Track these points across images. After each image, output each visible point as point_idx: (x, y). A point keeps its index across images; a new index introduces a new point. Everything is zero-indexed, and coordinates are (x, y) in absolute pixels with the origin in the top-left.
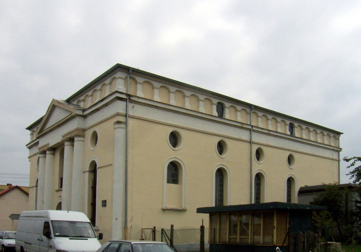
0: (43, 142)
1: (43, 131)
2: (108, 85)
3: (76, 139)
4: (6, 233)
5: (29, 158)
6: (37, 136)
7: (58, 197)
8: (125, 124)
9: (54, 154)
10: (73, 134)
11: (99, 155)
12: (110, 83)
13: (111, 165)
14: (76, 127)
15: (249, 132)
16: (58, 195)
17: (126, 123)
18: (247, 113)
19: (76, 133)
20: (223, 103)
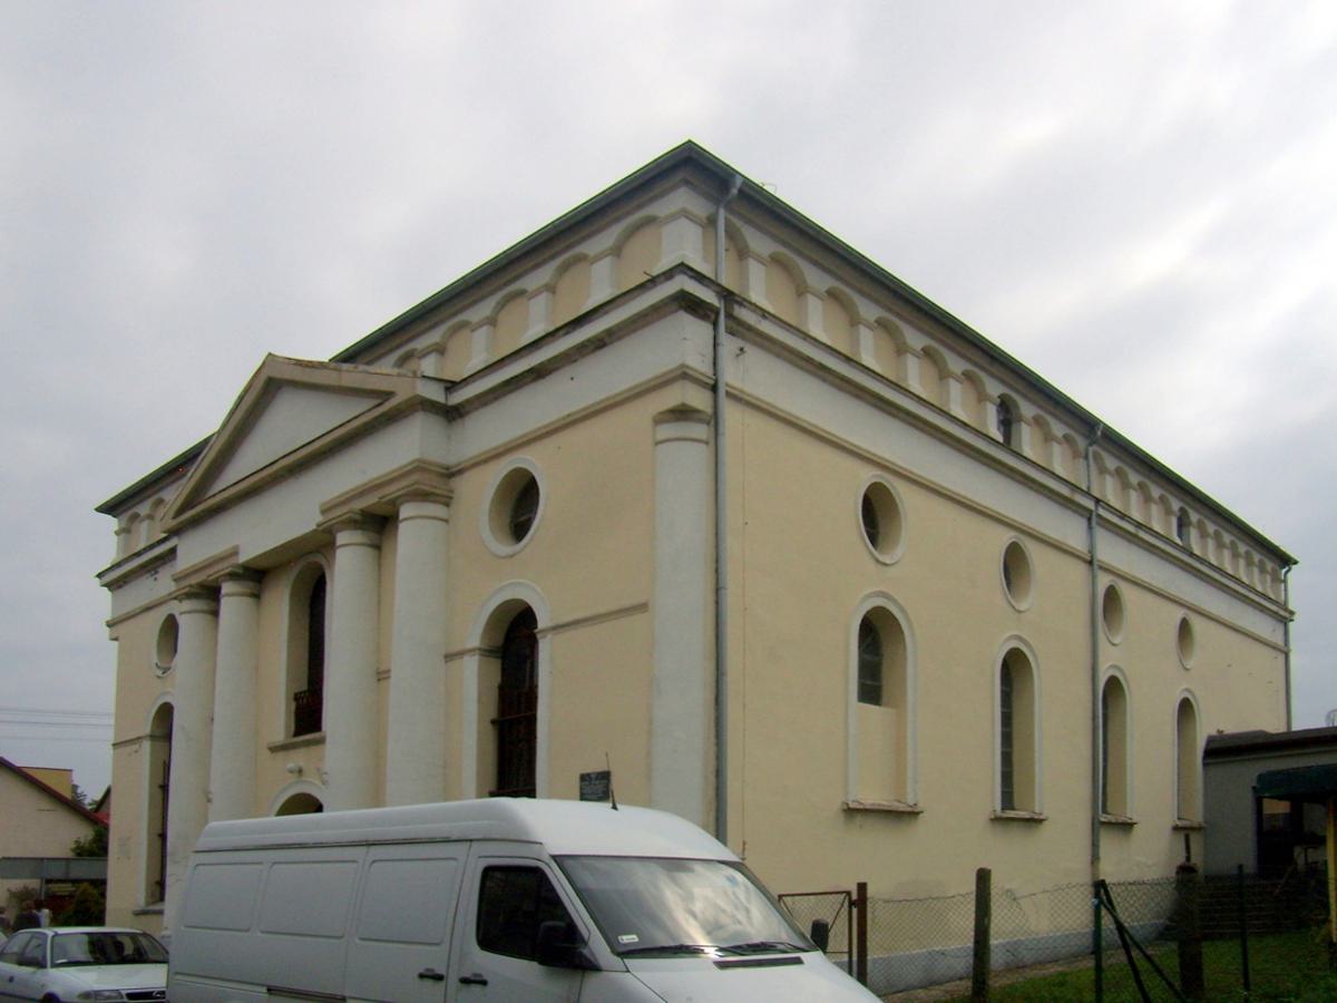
0: (196, 550)
1: (200, 503)
2: (481, 326)
3: (406, 511)
4: (56, 934)
5: (110, 625)
6: (171, 523)
7: (291, 772)
8: (708, 423)
9: (257, 596)
10: (392, 490)
11: (540, 578)
12: (617, 251)
13: (642, 607)
14: (418, 456)
15: (1083, 523)
16: (291, 765)
17: (714, 420)
18: (1076, 455)
19: (416, 483)
20: (1014, 401)
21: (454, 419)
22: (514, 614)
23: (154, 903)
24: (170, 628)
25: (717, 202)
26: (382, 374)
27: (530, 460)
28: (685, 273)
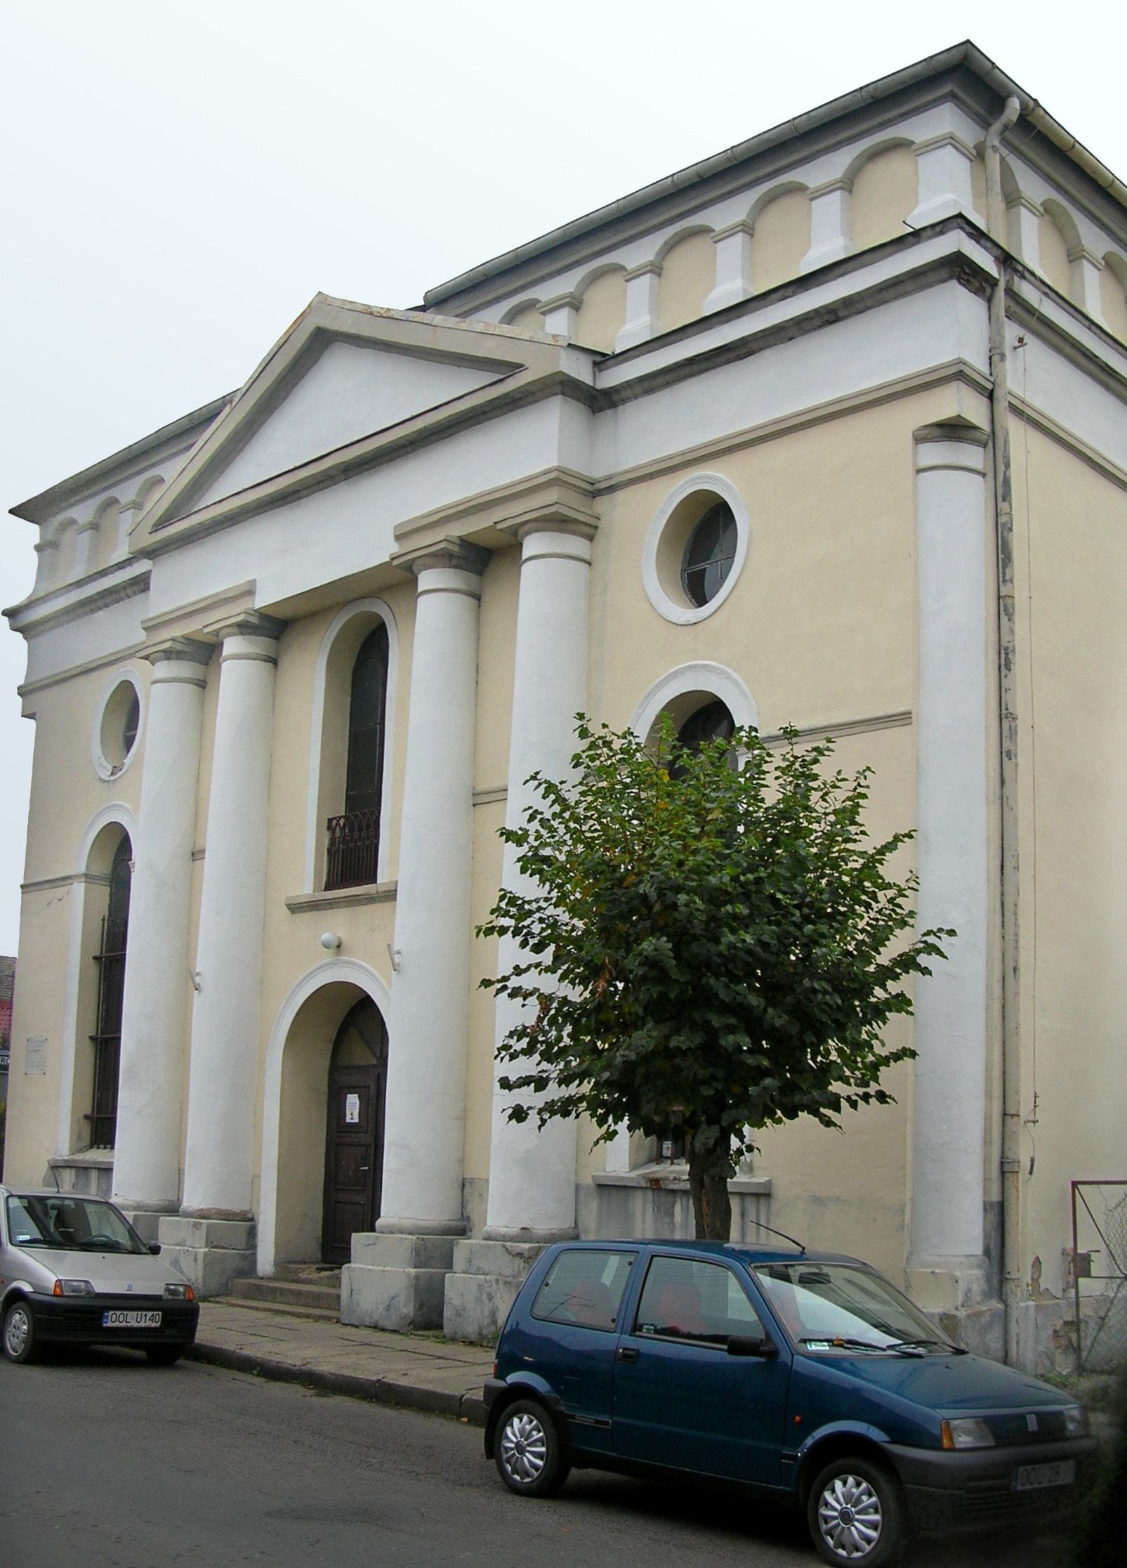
0: (194, 583)
3: (532, 545)
5: (22, 692)
7: (326, 946)
12: (848, 184)
13: (904, 718)
14: (553, 463)
16: (326, 936)
17: (991, 441)
21: (601, 409)
22: (694, 708)
23: (80, 1151)
24: (126, 710)
25: (986, 125)
26: (485, 329)
27: (720, 479)
28: (962, 229)
